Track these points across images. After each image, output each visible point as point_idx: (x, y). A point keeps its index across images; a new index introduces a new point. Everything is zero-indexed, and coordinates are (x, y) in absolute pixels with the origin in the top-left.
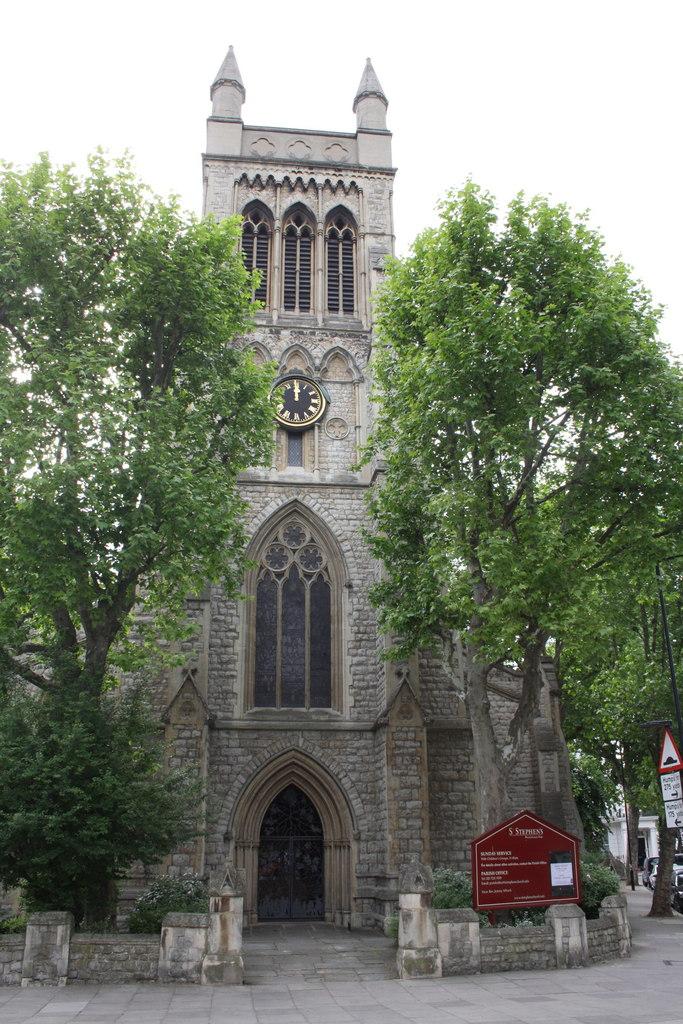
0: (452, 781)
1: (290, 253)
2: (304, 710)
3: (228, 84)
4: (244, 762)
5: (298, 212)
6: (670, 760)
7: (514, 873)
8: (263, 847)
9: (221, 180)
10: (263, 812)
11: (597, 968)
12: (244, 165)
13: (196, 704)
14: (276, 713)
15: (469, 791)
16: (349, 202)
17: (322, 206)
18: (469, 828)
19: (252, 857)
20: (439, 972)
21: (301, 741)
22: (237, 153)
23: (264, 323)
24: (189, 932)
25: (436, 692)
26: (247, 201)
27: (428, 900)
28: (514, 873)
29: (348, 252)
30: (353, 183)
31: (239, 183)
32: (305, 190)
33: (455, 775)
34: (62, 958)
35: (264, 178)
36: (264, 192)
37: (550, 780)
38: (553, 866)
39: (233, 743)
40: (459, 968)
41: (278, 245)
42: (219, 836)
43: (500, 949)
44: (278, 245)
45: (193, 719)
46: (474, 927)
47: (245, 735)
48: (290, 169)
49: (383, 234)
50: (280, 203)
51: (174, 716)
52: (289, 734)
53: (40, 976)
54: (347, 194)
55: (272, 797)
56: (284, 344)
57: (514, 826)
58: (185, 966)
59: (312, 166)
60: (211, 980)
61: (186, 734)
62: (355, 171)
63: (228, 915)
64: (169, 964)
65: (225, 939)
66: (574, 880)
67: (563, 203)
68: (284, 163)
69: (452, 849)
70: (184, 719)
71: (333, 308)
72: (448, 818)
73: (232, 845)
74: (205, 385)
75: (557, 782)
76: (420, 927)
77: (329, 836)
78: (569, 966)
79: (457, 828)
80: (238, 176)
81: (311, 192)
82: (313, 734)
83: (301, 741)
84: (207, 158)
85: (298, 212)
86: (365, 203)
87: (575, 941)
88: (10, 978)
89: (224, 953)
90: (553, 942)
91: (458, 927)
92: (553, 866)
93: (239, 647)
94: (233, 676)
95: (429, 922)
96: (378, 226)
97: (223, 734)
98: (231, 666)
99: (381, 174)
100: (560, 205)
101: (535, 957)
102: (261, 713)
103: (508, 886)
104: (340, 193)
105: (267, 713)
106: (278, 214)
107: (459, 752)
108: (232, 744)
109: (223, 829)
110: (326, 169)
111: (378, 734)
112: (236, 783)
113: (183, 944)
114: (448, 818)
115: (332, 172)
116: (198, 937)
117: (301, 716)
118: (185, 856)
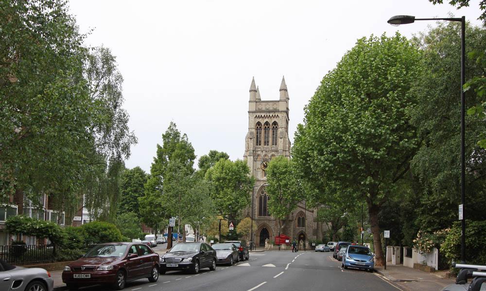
1: (265, 132)
8: (261, 236)
17: (271, 121)
19: (259, 238)
27: (268, 243)
29: (276, 131)
32: (268, 118)
35: (260, 116)
40: (271, 249)
44: (263, 131)
50: (263, 122)
56: (264, 154)
59: (270, 112)
74: (371, 169)
77: (270, 235)
85: (267, 123)
87: (284, 248)
106: (271, 124)
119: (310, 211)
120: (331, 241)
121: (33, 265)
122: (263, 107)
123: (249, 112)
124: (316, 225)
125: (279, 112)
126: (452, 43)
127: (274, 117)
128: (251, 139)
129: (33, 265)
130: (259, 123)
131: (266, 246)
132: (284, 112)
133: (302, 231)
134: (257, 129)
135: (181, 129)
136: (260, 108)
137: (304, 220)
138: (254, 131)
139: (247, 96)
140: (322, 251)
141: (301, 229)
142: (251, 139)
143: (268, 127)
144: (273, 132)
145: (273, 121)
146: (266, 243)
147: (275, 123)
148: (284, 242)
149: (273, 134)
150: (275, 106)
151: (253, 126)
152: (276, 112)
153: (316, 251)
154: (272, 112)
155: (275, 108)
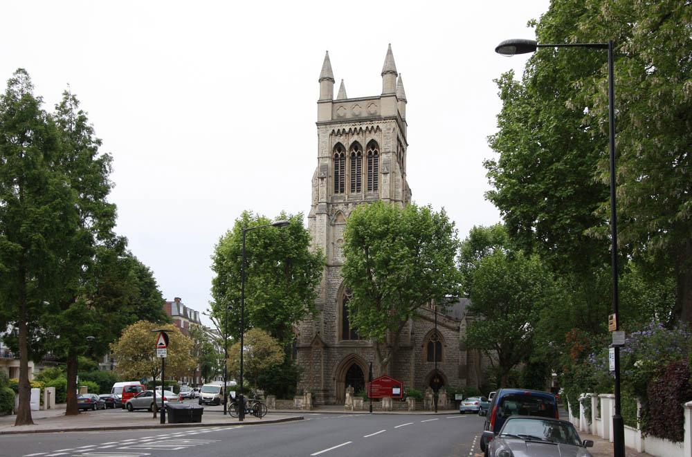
0: (404, 363)
1: (353, 164)
2: (357, 341)
3: (327, 79)
4: (338, 358)
5: (356, 145)
6: (161, 344)
7: (380, 390)
10: (346, 371)
12: (333, 125)
13: (320, 342)
16: (373, 136)
17: (364, 141)
23: (342, 201)
26: (335, 143)
27: (351, 395)
28: (380, 390)
29: (376, 161)
30: (378, 126)
31: (331, 135)
41: (348, 163)
42: (332, 378)
44: (348, 163)
46: (362, 401)
48: (351, 124)
50: (347, 142)
51: (313, 345)
54: (375, 132)
55: (348, 367)
59: (361, 121)
67: (64, 92)
68: (348, 121)
71: (369, 189)
75: (466, 361)
78: (86, 409)
80: (331, 131)
81: (361, 135)
85: (356, 145)
87: (387, 405)
89: (306, 404)
91: (358, 401)
93: (336, 322)
100: (64, 94)
104: (373, 132)
108: (335, 352)
115: (369, 122)
116: (302, 401)
119: (453, 329)
122: (347, 112)
124: (465, 356)
125: (380, 118)
127: (370, 132)
128: (322, 179)
130: (339, 147)
131: (347, 402)
132: (390, 118)
134: (336, 159)
137: (439, 345)
138: (329, 162)
139: (315, 91)
140: (476, 412)
142: (322, 179)
143: (359, 154)
144: (370, 163)
145: (368, 140)
148: (390, 393)
149: (370, 168)
150: (372, 109)
152: (375, 119)
153: (463, 413)
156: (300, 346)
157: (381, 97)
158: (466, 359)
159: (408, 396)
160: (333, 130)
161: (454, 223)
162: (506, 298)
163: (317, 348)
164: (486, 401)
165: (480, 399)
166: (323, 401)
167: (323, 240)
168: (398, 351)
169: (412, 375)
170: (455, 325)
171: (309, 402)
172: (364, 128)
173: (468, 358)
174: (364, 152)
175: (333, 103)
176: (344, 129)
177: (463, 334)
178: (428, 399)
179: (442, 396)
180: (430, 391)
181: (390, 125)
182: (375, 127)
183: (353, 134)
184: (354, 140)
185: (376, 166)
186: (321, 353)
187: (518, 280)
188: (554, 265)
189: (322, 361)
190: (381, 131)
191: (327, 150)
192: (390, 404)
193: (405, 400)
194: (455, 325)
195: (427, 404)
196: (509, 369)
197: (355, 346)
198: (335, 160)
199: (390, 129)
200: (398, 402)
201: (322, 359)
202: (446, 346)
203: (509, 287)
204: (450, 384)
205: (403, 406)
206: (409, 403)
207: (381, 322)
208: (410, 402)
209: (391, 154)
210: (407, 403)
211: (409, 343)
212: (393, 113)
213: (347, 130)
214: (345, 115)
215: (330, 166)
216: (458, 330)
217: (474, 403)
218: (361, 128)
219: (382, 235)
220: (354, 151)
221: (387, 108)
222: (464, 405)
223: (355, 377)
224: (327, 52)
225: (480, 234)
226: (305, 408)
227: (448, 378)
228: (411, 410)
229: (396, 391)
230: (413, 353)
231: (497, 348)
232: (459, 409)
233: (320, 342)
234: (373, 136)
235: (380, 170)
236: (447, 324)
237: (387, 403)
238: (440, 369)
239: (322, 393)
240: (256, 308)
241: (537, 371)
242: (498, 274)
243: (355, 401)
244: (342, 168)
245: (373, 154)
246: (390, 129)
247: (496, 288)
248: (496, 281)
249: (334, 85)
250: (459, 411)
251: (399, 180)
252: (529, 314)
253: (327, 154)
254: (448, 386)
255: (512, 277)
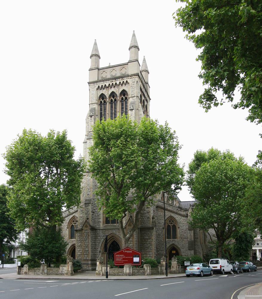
0: (147, 239)
2: (116, 224)
3: (96, 56)
5: (113, 94)
9: (93, 89)
11: (153, 276)
12: (98, 83)
13: (88, 225)
14: (110, 225)
15: (151, 241)
16: (124, 87)
17: (118, 91)
18: (151, 250)
20: (101, 275)
21: (114, 231)
22: (96, 79)
24: (63, 267)
25: (144, 219)
27: (100, 263)
28: (124, 259)
29: (126, 103)
30: (127, 81)
31: (98, 89)
33: (148, 238)
34: (46, 271)
36: (104, 90)
37: (191, 238)
38: (134, 258)
39: (100, 232)
41: (108, 106)
42: (98, 251)
43: (113, 272)
44: (108, 106)
45: (88, 228)
47: (103, 231)
49: (134, 96)
50: (107, 93)
51: (84, 228)
52: (112, 230)
53: (43, 273)
54: (125, 85)
57: (124, 250)
58: (63, 273)
59: (116, 78)
60: (66, 275)
61: (86, 232)
62: (127, 77)
63: (69, 265)
64: (61, 272)
65: (68, 268)
66: (21, 265)
69: (147, 254)
70: (86, 228)
72: (146, 247)
73: (101, 253)
76: (99, 268)
79: (148, 250)
80: (97, 87)
81: (116, 88)
82: (117, 230)
83: (114, 231)
84: (89, 83)
85: (113, 94)
86: (130, 87)
87: (128, 271)
88: (39, 274)
89: (68, 271)
90: (124, 271)
92: (134, 258)
94: (100, 218)
95: (100, 267)
96: (133, 94)
97: (99, 231)
98: (100, 216)
99: (134, 76)
101: (120, 274)
102: (107, 225)
103: (122, 261)
104: (124, 85)
105: (108, 225)
107: (149, 232)
109: (99, 250)
110: (119, 78)
111: (152, 226)
112: (101, 241)
113: (63, 269)
114: (146, 247)
115: (121, 79)
117: (115, 226)
118: (87, 255)
119: (183, 216)
120: (217, 257)
121: (166, 237)
122: (108, 74)
123: (89, 83)
124: (192, 234)
125: (128, 76)
126: (235, 228)
127: (122, 85)
128: (91, 116)
129: (166, 237)
130: (102, 96)
131: (97, 269)
132: (135, 75)
133: (173, 244)
134: (101, 104)
135: (69, 138)
136: (104, 77)
137: (174, 227)
138: (96, 107)
139: (88, 63)
140: (199, 276)
141: (170, 242)
142: (91, 116)
143: (115, 100)
144: (122, 105)
145: (121, 90)
146: (98, 263)
147: (124, 93)
148: (131, 261)
149: (122, 108)
150: (123, 71)
151: (95, 100)
152: (125, 77)
153: (188, 276)
154: (119, 78)
155: (123, 73)
156: (78, 229)
157: (128, 62)
158: (193, 236)
159: (146, 263)
160: (99, 86)
161: (175, 132)
162: (219, 189)
163: (87, 230)
164: (206, 267)
165: (201, 265)
166: (90, 268)
167: (81, 150)
168: (143, 231)
169: (153, 247)
170: (184, 213)
171: (70, 269)
172: (118, 83)
173: (194, 236)
174: (118, 98)
175: (99, 70)
176: (105, 85)
177: (190, 218)
178: (162, 266)
179: (174, 263)
180: (164, 260)
181: (134, 79)
182: (125, 82)
183: (111, 87)
184: (112, 91)
185: (126, 107)
186: (90, 234)
187: (225, 176)
188: (252, 173)
189: (90, 239)
190: (129, 83)
191: (95, 99)
192: (130, 270)
193: (143, 267)
194: (184, 213)
195: (161, 269)
196: (223, 242)
197: (114, 228)
198: (100, 105)
199: (134, 82)
200: (138, 268)
201: (90, 237)
202: (179, 228)
203: (220, 182)
204: (183, 254)
205: (141, 271)
206: (146, 269)
207: (119, 205)
208: (147, 268)
209: (136, 97)
210: (144, 269)
211: (151, 226)
212: (135, 72)
213: (107, 85)
214: (106, 76)
215: (96, 109)
216: (187, 216)
217: (196, 268)
218: (116, 83)
219: (118, 137)
220: (112, 98)
221: (132, 69)
222: (189, 270)
223: (112, 251)
224: (95, 40)
225: (200, 155)
226: (67, 274)
227: (182, 250)
228: (148, 275)
229: (136, 259)
230: (154, 233)
231: (214, 227)
232: (185, 272)
233: (88, 225)
234: (124, 87)
235: (129, 109)
236: (180, 212)
237: (128, 269)
238: (176, 243)
239: (90, 262)
240: (28, 197)
241: (243, 245)
242: (211, 173)
243: (103, 268)
244: (105, 109)
245: (124, 99)
246: (134, 82)
247: (210, 183)
248: (210, 178)
249: (100, 60)
250: (185, 275)
251: (141, 115)
252: (235, 200)
253: (95, 101)
254: (182, 256)
255: (221, 174)
